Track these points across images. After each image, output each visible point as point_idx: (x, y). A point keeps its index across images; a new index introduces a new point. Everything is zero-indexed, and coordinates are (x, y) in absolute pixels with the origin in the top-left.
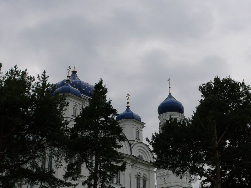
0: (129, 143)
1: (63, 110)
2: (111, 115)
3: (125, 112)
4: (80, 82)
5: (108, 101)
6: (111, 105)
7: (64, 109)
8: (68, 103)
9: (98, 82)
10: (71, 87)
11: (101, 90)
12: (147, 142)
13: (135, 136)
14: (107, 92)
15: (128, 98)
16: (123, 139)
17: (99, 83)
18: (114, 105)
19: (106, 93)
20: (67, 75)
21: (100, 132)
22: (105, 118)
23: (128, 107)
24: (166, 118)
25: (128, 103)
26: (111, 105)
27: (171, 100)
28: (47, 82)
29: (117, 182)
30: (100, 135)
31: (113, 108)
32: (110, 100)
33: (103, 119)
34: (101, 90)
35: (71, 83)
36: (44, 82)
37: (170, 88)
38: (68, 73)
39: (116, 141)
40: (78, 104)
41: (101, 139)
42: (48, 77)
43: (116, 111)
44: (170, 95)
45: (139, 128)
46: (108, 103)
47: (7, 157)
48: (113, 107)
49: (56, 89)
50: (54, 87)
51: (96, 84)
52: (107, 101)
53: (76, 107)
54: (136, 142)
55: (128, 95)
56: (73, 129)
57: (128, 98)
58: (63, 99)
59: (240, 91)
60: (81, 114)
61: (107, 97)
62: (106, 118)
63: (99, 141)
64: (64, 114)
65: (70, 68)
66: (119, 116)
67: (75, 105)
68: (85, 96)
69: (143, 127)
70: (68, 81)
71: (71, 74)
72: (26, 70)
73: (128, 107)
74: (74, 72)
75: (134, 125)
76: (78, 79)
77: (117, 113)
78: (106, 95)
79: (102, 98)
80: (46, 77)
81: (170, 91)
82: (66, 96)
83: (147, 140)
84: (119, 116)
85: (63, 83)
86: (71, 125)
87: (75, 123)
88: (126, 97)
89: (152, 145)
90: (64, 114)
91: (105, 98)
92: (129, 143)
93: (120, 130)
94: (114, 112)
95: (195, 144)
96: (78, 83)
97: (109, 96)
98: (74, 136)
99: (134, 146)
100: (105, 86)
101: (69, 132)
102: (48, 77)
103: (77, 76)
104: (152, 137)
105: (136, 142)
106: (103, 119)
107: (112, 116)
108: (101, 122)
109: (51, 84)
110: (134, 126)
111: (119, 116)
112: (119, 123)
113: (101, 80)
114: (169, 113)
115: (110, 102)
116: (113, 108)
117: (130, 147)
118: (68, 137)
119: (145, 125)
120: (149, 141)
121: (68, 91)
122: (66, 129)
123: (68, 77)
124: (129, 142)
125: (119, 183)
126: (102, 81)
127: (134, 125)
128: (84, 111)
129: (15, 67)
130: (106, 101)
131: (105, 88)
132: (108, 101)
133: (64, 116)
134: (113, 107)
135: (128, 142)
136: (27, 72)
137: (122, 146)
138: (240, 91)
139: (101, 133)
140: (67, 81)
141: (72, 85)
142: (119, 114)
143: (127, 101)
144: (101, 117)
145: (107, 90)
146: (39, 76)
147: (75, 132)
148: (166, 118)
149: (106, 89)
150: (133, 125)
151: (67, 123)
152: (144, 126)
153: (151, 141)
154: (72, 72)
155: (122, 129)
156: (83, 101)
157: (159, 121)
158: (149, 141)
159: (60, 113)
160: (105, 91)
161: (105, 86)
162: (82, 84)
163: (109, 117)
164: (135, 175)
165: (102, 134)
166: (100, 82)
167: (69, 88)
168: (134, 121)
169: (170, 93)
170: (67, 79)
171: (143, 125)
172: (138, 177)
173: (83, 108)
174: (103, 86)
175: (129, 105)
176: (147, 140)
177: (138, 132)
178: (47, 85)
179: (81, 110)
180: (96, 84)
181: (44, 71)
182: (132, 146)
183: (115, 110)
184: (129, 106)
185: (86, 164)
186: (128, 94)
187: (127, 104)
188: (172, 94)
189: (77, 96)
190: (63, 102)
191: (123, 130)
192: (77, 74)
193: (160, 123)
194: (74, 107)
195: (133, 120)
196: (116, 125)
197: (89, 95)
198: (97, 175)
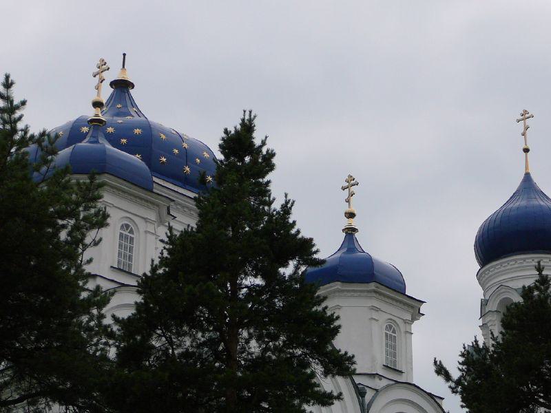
0: (356, 386)
1: (85, 247)
2: (292, 264)
3: (338, 255)
4: (148, 128)
5: (277, 206)
6: (291, 221)
7: (88, 240)
8: (106, 216)
9: (234, 125)
10: (109, 146)
11: (247, 159)
12: (441, 379)
13: (381, 358)
14: (271, 167)
15: (527, 128)
16: (340, 365)
17: (239, 127)
18: (304, 223)
19: (267, 173)
20: (94, 97)
21: (245, 334)
22: (264, 277)
23: (350, 232)
24: (512, 279)
25: (351, 215)
26: (291, 221)
28: (20, 125)
30: (243, 350)
31: (300, 236)
32: (287, 202)
33: (259, 281)
34: (247, 159)
35: (110, 130)
36: (8, 127)
37: (526, 150)
38: (97, 88)
39: (313, 375)
41: (247, 368)
42: (23, 103)
43: (314, 249)
45: (398, 321)
46: (278, 213)
48: (298, 232)
49: (54, 153)
50: (47, 142)
51: (226, 131)
52: (273, 206)
53: (131, 232)
54: (384, 383)
55: (351, 182)
56: (127, 325)
57: (527, 128)
58: (90, 195)
60: (164, 262)
61: (271, 187)
62: (270, 275)
63: (240, 374)
64: (90, 261)
65: (103, 66)
66: (324, 266)
67: (127, 226)
68: (176, 188)
69: (414, 319)
70: (96, 123)
71: (106, 93)
73: (350, 232)
74: (122, 86)
75: (377, 310)
76: (139, 113)
77: (315, 256)
78: (266, 180)
79: (251, 194)
80: (15, 103)
81: (527, 168)
82: (101, 185)
83: (441, 370)
84: (326, 269)
85: (74, 133)
86: (123, 305)
87: (139, 299)
88: (344, 189)
89: (461, 393)
90: (90, 261)
91: (263, 192)
92: (356, 386)
93: (326, 328)
94: (303, 248)
96: (137, 131)
97: (279, 185)
98: (134, 353)
99: (377, 398)
100: (264, 143)
101: (111, 335)
102: (23, 103)
103: (134, 105)
104: (462, 359)
105: (384, 383)
106: (259, 281)
107: (297, 268)
108: (248, 295)
109: (35, 131)
110: (375, 315)
111: (324, 266)
112: (325, 298)
113: (247, 117)
114: (531, 259)
115: (286, 209)
116: (300, 236)
117: (362, 404)
118: (104, 357)
119: (423, 309)
120: (448, 377)
121: (95, 166)
122: (99, 325)
123: (97, 104)
124: (357, 380)
126: (250, 120)
128: (180, 246)
130: (270, 204)
131: (264, 150)
132: (277, 206)
133: (88, 269)
134: (298, 232)
135: (353, 381)
137: (339, 397)
139: (247, 341)
140: (92, 121)
141: (116, 143)
142: (323, 262)
144: (246, 274)
145: (274, 160)
147: (139, 338)
148: (512, 279)
149: (271, 155)
151: (100, 298)
152: (417, 314)
153: (456, 375)
154: (114, 84)
155: (336, 323)
156: (166, 210)
157: (478, 293)
158: (448, 377)
159: (72, 256)
160: (267, 163)
161: (264, 143)
162: (155, 133)
163: (282, 270)
165: (253, 343)
166: (243, 124)
167: (104, 151)
168: (375, 292)
170: (91, 113)
171: (414, 307)
173: (171, 239)
174: (257, 142)
175: (354, 223)
176: (441, 370)
177: (394, 338)
178: (17, 137)
179: (161, 245)
180: (226, 131)
181: (7, 77)
182: (368, 398)
183: (307, 244)
184: (355, 230)
186: (351, 178)
188: (535, 178)
189: (138, 186)
190: (87, 209)
191: (340, 327)
192: (131, 91)
193: (484, 303)
195: (372, 286)
196: (315, 305)
197: (195, 182)
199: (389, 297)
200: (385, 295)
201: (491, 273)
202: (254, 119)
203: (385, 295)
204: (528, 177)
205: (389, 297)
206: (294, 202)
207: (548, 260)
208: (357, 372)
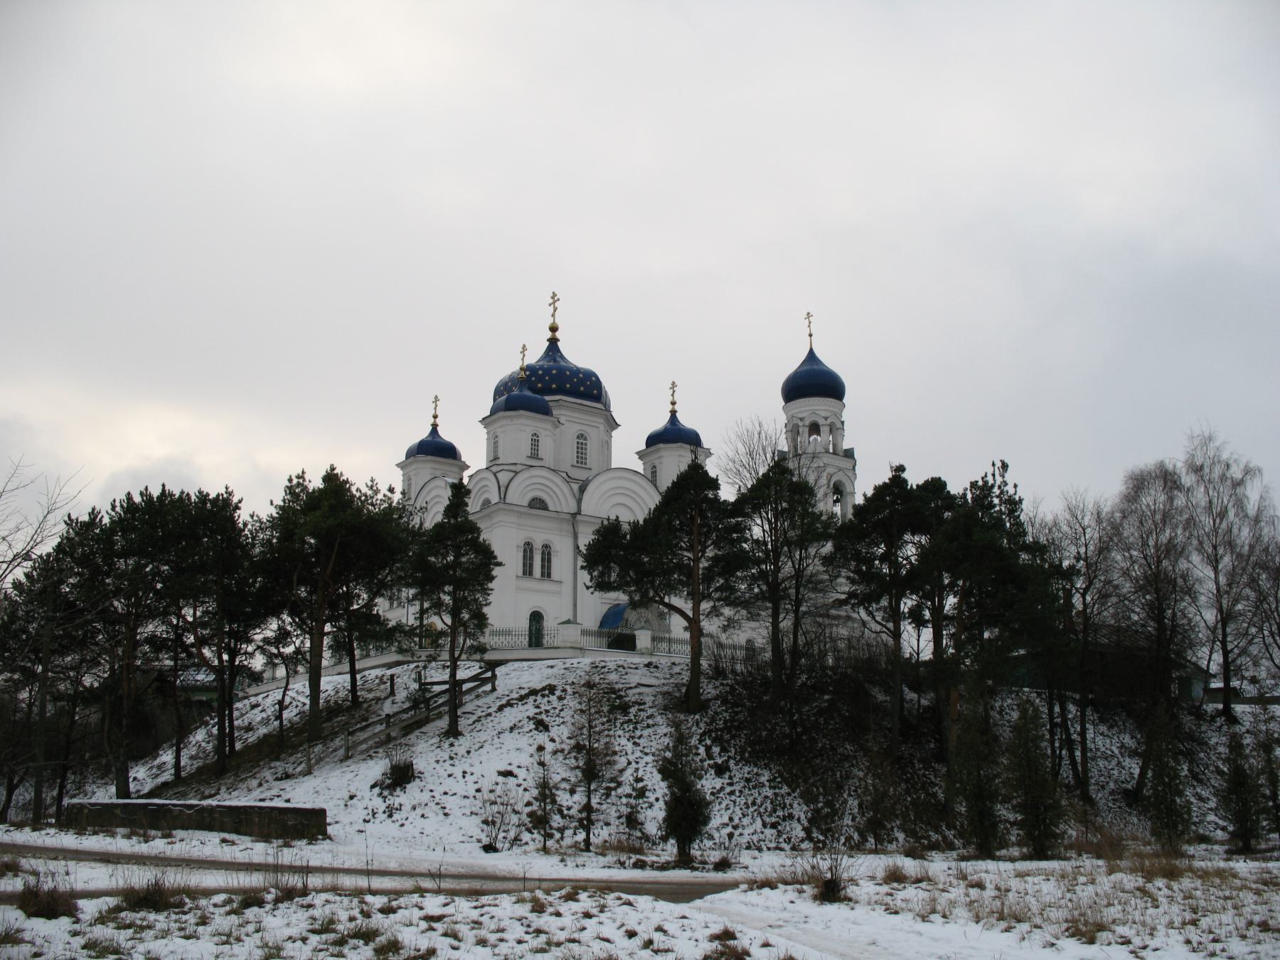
15: (810, 323)
23: (673, 413)
24: (800, 412)
27: (815, 367)
29: (543, 575)
37: (810, 335)
40: (540, 430)
44: (811, 356)
59: (172, 663)
73: (673, 413)
75: (683, 456)
95: (234, 578)
110: (681, 459)
125: (549, 575)
127: (683, 456)
138: (172, 663)
146: (502, 769)
148: (800, 412)
150: (680, 456)
164: (518, 547)
169: (811, 350)
187: (549, 334)
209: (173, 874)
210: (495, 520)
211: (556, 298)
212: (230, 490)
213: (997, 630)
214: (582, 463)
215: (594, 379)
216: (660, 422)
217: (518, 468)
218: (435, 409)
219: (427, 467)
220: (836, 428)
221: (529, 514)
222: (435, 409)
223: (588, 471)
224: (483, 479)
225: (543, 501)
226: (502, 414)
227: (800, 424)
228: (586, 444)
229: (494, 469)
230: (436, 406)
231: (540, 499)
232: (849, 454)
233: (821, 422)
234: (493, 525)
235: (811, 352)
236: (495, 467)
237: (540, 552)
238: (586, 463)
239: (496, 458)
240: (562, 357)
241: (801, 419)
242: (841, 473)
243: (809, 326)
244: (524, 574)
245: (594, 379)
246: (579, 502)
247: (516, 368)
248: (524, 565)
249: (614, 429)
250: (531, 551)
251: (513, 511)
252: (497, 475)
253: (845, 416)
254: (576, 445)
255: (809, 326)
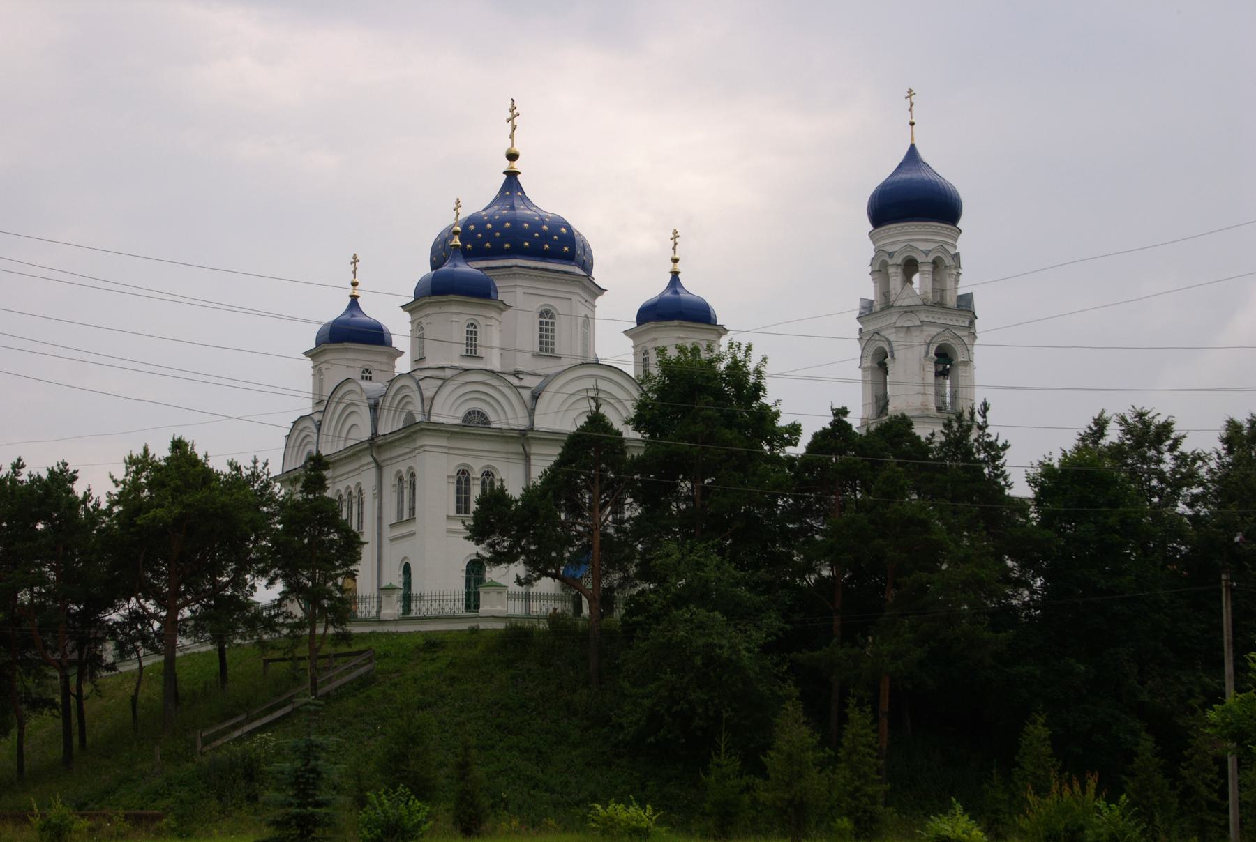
15: (912, 104)
31: (24, 476)
37: (912, 124)
44: (912, 155)
47: (326, 628)
65: (405, 558)
72: (1007, 441)
81: (912, 139)
129: (1007, 441)
136: (1008, 445)
143: (506, 145)
169: (913, 148)
172: (70, 654)
175: (517, 165)
184: (516, 173)
185: (298, 601)
187: (506, 165)
188: (919, 148)
194: (467, 331)
198: (1219, 581)
199: (707, 329)
200: (688, 327)
201: (885, 234)
202: (206, 460)
203: (688, 327)
204: (913, 148)
205: (707, 329)
206: (193, 441)
207: (907, 227)
208: (535, 429)
209: (930, 822)
210: (419, 443)
211: (515, 112)
212: (77, 475)
213: (859, 634)
214: (547, 350)
215: (563, 230)
216: (655, 288)
217: (448, 373)
218: (354, 272)
219: (347, 363)
220: (945, 265)
221: (463, 433)
222: (354, 272)
223: (555, 360)
224: (403, 387)
225: (483, 415)
226: (427, 300)
227: (890, 262)
228: (553, 324)
229: (419, 375)
230: (355, 269)
231: (478, 412)
232: (965, 303)
233: (920, 258)
234: (415, 449)
235: (913, 148)
236: (418, 373)
237: (479, 482)
238: (552, 351)
239: (422, 359)
240: (524, 198)
241: (891, 255)
242: (947, 333)
243: (910, 110)
244: (458, 511)
245: (563, 230)
246: (531, 413)
247: (451, 221)
248: (458, 500)
249: (596, 296)
250: (467, 481)
251: (441, 431)
252: (421, 383)
253: (963, 245)
254: (539, 326)
255: (910, 110)
